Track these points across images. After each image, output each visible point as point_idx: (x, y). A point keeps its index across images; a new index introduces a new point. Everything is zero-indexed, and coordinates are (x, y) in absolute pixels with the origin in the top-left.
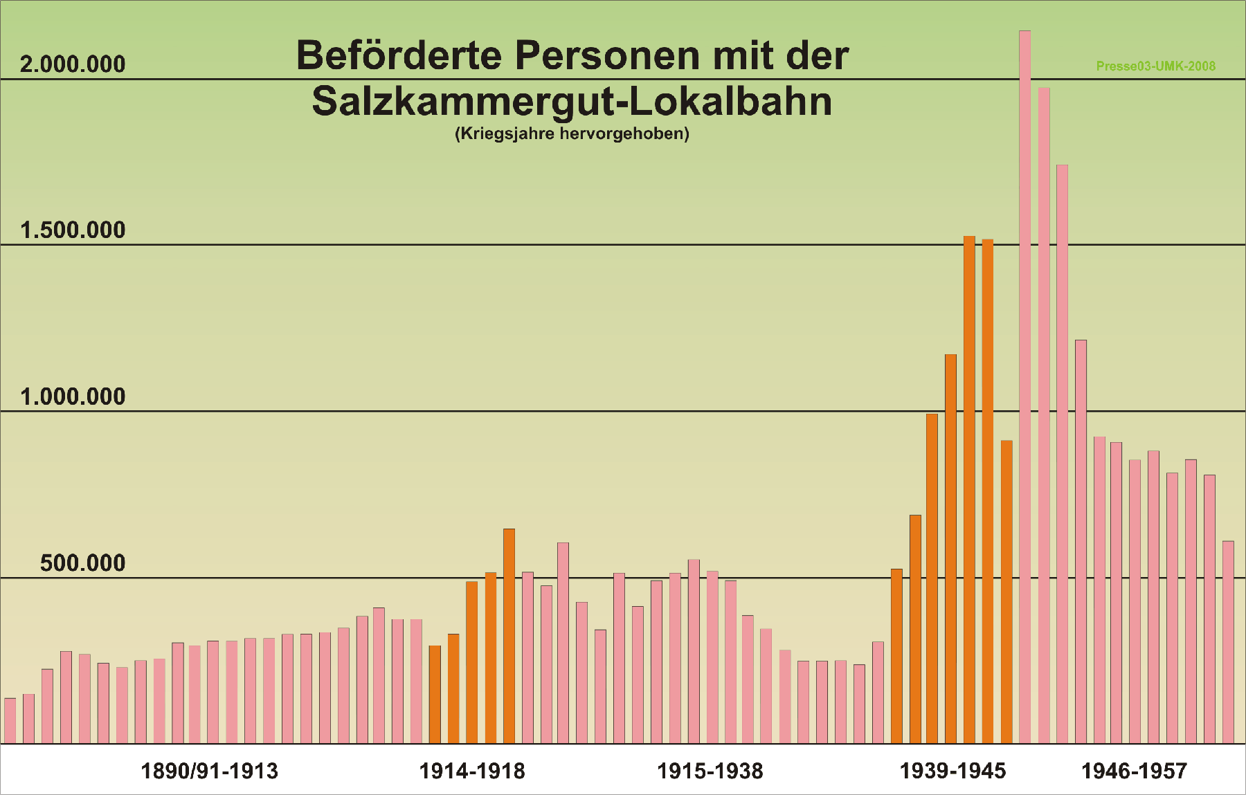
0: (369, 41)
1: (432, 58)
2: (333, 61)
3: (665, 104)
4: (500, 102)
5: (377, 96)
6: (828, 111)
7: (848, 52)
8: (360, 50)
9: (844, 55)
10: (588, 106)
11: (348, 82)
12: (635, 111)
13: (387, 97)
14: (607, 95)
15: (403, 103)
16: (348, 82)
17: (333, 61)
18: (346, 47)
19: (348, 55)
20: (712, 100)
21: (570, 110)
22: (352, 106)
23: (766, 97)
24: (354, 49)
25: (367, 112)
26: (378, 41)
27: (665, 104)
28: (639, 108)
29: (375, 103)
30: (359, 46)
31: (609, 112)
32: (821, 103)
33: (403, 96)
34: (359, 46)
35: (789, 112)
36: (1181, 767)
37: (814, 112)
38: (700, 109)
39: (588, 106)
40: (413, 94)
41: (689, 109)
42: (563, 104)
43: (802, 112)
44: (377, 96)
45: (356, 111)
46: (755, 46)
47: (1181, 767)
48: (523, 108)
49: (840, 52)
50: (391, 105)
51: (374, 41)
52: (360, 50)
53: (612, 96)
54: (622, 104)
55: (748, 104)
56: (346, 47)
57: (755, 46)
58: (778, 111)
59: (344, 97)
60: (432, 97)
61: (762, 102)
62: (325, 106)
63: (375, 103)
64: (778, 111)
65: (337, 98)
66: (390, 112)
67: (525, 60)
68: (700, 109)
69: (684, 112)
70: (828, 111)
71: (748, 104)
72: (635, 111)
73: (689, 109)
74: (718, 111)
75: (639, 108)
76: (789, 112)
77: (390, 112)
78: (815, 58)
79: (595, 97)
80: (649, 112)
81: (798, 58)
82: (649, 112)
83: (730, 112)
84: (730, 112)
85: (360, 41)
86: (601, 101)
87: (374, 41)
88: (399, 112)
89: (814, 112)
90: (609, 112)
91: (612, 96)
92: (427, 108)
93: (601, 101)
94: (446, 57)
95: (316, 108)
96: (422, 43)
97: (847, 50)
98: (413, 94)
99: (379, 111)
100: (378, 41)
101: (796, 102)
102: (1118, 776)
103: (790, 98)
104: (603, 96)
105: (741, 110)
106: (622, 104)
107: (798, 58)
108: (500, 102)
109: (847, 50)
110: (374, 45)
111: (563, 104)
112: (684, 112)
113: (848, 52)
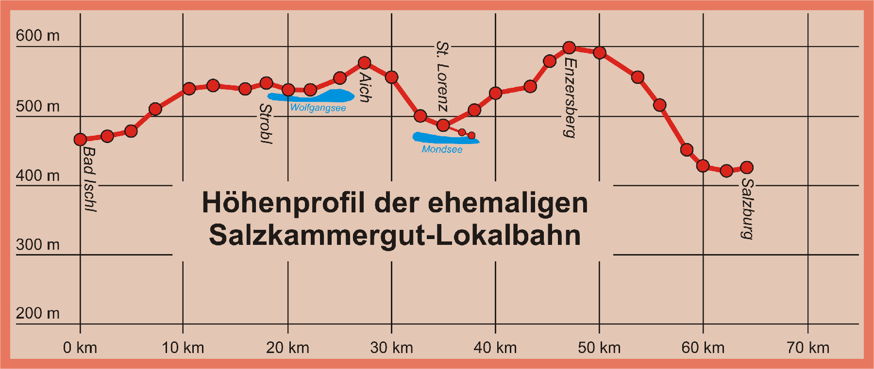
0: (228, 193)
1: (395, 205)
2: (561, 207)
3: (462, 237)
4: (343, 236)
5: (255, 231)
6: (578, 242)
7: (418, 200)
8: (348, 199)
9: (416, 202)
10: (406, 239)
11: (234, 221)
12: (440, 242)
13: (263, 232)
14: (420, 231)
15: (274, 236)
16: (234, 221)
17: (561, 207)
18: (338, 196)
19: (340, 203)
20: (292, 234)
21: (393, 241)
22: (238, 238)
23: (534, 232)
24: (344, 198)
25: (248, 243)
26: (234, 193)
27: (462, 237)
28: (443, 240)
29: (254, 236)
30: (348, 195)
31: (421, 243)
32: (573, 236)
33: (275, 232)
34: (348, 195)
35: (550, 243)
36: (791, 344)
37: (568, 243)
38: (283, 241)
39: (406, 239)
40: (485, 231)
41: (478, 241)
42: (388, 237)
43: (560, 243)
44: (255, 231)
45: (240, 242)
46: (533, 196)
47: (791, 344)
48: (360, 240)
49: (413, 200)
50: (266, 238)
51: (231, 193)
52: (348, 199)
53: (423, 231)
54: (430, 237)
55: (521, 237)
56: (338, 196)
57: (533, 196)
58: (542, 242)
59: (232, 232)
60: (295, 232)
61: (530, 236)
62: (218, 239)
63: (254, 236)
64: (542, 242)
65: (227, 232)
66: (265, 243)
67: (209, 204)
68: (283, 240)
69: (475, 243)
70: (578, 242)
71: (521, 237)
72: (440, 242)
73: (478, 241)
74: (240, 242)
75: (443, 240)
76: (550, 243)
77: (265, 243)
78: (395, 205)
79: (411, 232)
80: (450, 243)
81: (383, 205)
82: (450, 243)
83: (508, 243)
84: (508, 243)
85: (348, 192)
86: (415, 235)
87: (231, 193)
88: (271, 243)
89: (568, 243)
90: (421, 243)
91: (423, 231)
92: (291, 240)
93: (415, 235)
94: (271, 204)
95: (212, 240)
96: (388, 193)
97: (418, 199)
98: (485, 231)
99: (256, 242)
100: (234, 193)
101: (555, 236)
102: (482, 351)
103: (551, 232)
104: (417, 231)
105: (516, 242)
106: (430, 237)
107: (383, 205)
108: (343, 236)
109: (418, 199)
110: (231, 195)
111: (388, 237)
112: (475, 243)
113: (418, 200)
